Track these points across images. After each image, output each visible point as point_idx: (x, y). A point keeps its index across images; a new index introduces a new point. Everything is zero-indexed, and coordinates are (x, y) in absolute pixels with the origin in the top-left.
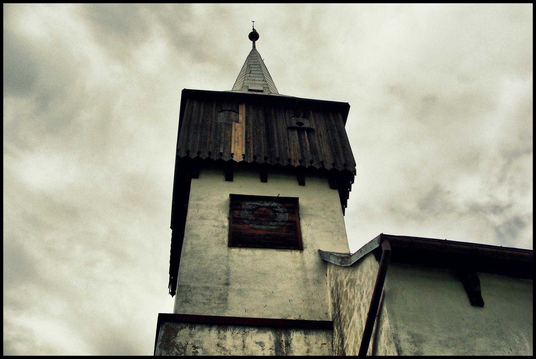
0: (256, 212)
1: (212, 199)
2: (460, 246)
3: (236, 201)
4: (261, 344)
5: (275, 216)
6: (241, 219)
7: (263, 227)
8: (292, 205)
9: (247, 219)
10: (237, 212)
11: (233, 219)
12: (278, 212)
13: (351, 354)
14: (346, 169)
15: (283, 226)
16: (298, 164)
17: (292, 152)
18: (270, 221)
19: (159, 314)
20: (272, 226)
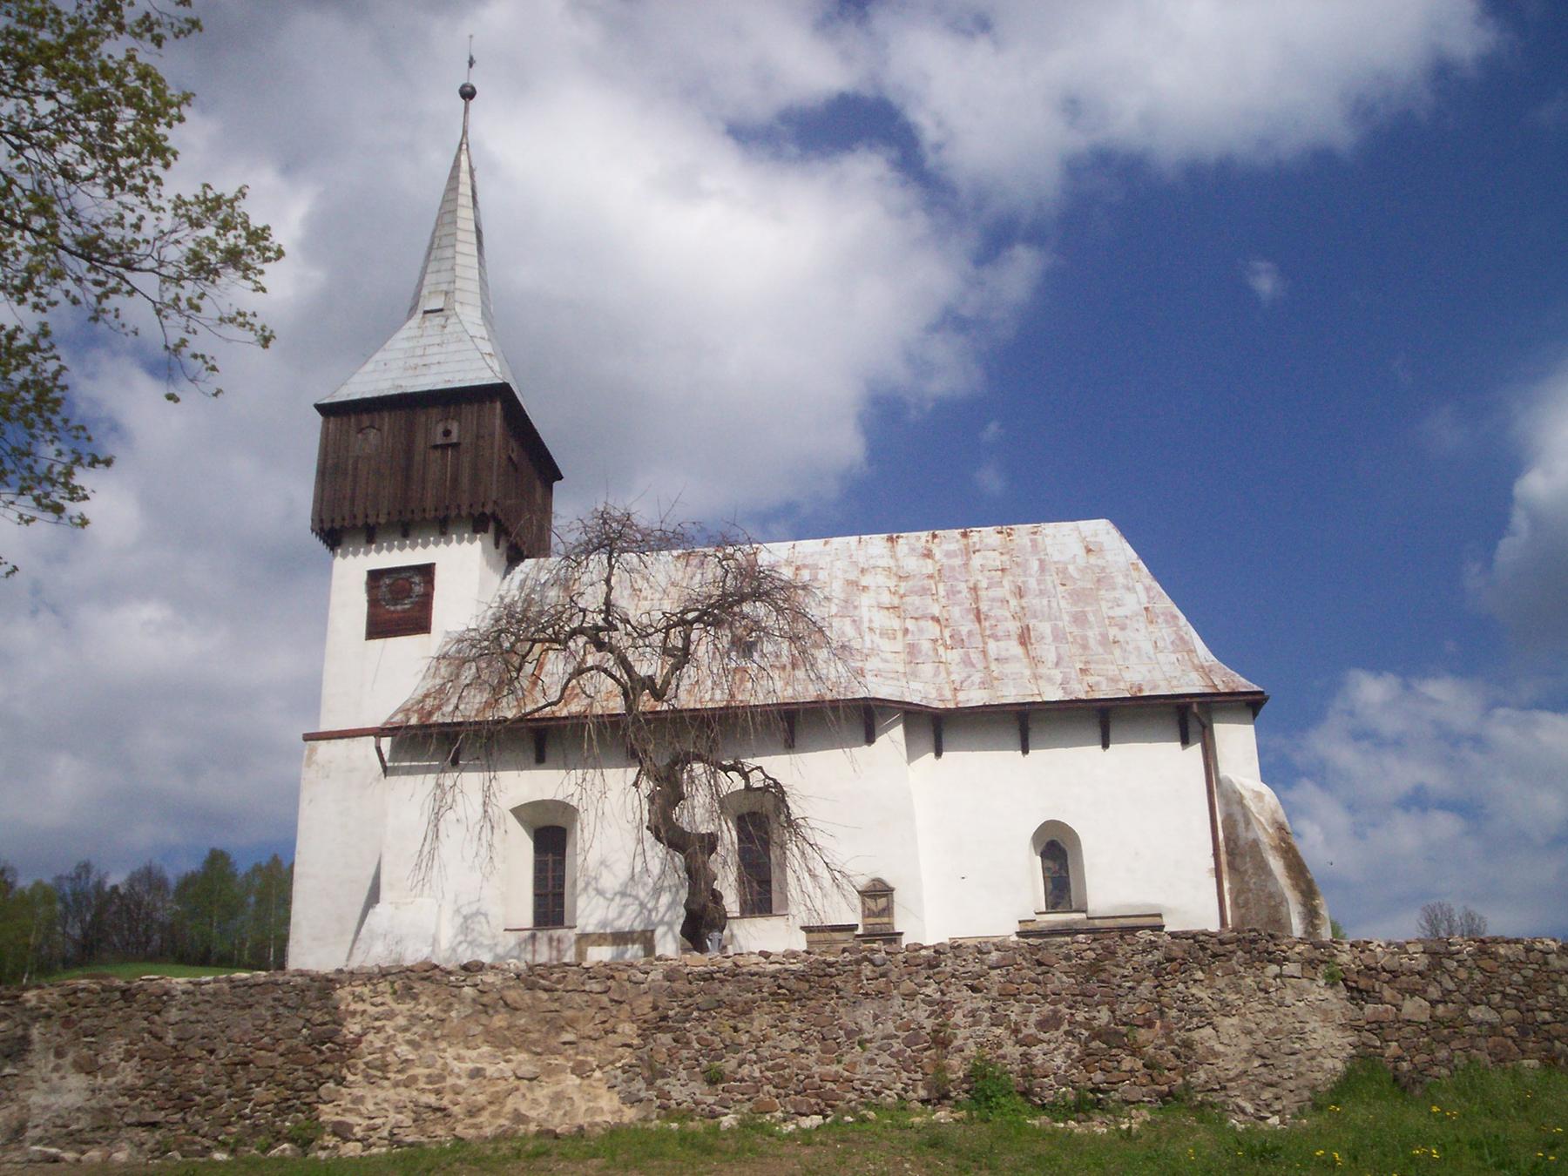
1: (351, 572)
3: (375, 576)
5: (411, 589)
7: (399, 608)
8: (426, 572)
11: (373, 603)
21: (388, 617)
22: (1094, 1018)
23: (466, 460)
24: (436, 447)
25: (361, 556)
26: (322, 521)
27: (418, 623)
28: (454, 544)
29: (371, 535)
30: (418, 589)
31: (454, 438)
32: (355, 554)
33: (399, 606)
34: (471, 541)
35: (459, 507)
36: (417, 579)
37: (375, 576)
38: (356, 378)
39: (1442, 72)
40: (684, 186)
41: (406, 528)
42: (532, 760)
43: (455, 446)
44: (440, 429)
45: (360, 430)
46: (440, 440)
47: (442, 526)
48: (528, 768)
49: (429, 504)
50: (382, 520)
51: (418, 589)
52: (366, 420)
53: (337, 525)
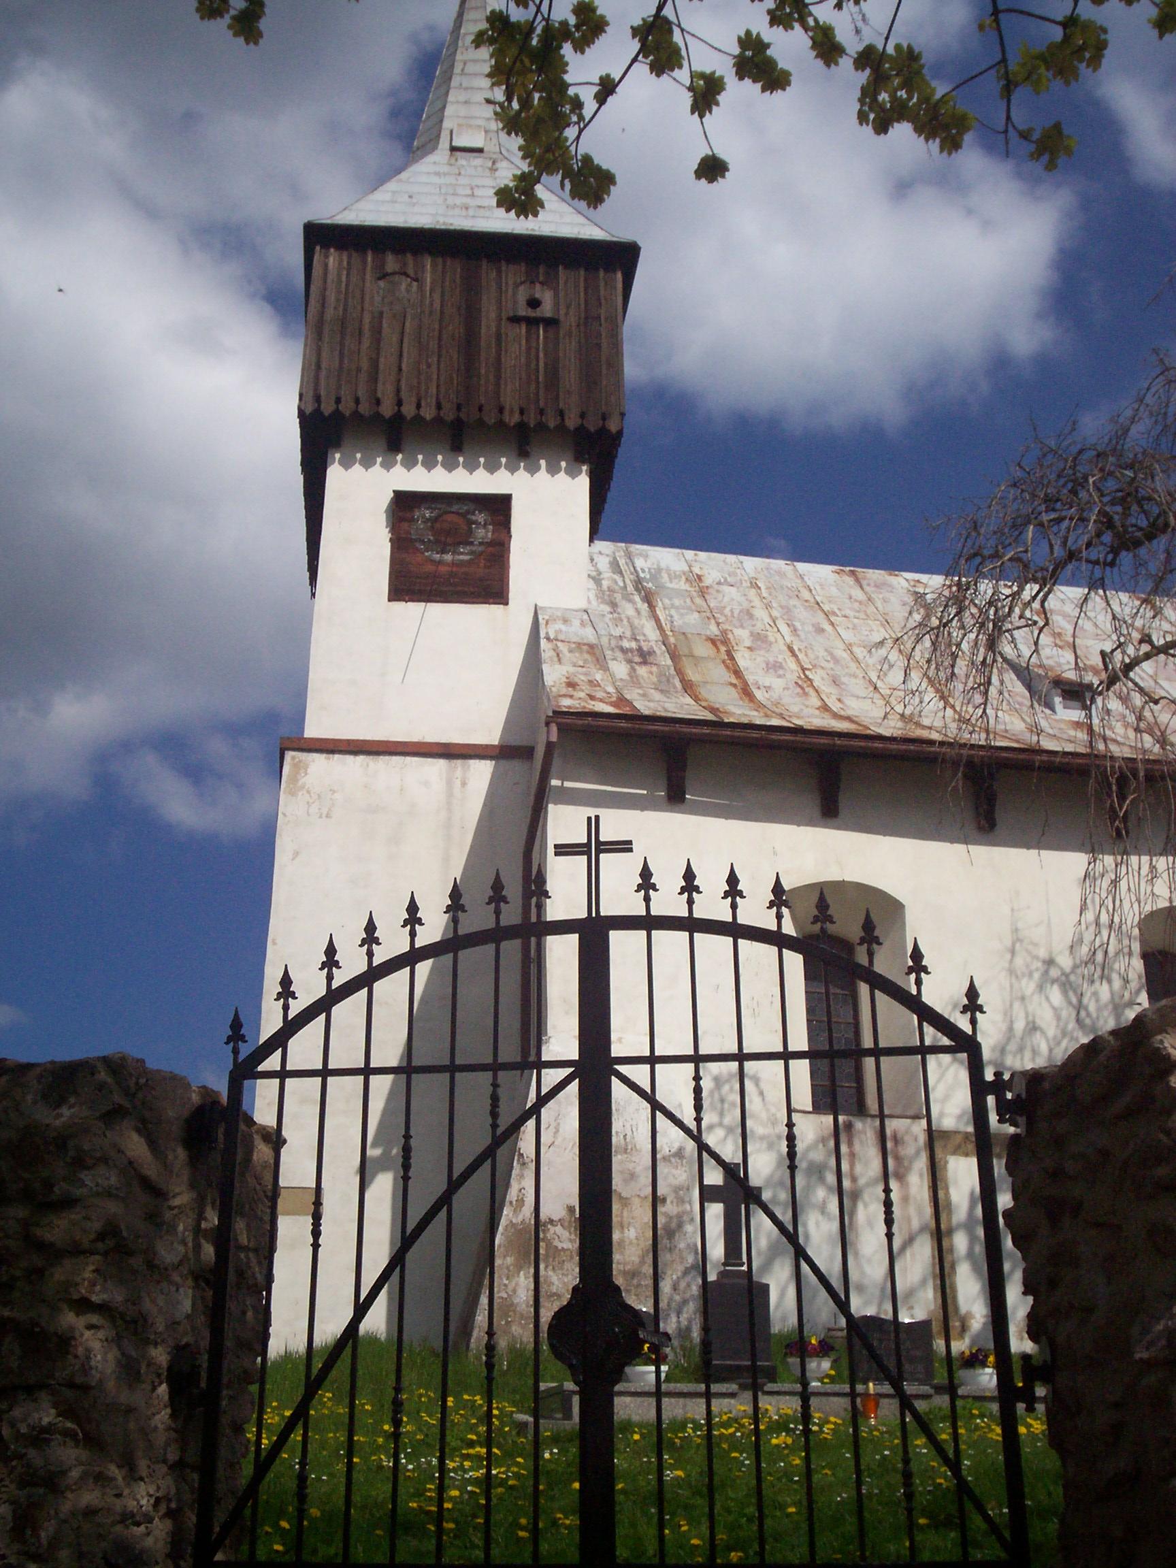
0: (438, 525)
1: (363, 491)
2: (686, 729)
3: (404, 503)
4: (426, 784)
5: (470, 531)
6: (411, 540)
7: (448, 557)
8: (499, 507)
9: (423, 542)
10: (405, 525)
11: (401, 543)
12: (475, 522)
13: (263, 1559)
14: (604, 426)
15: (481, 554)
16: (516, 418)
17: (509, 388)
18: (459, 543)
19: (346, 469)
20: (462, 553)
21: (430, 568)
22: (1030, 1409)
23: (569, 350)
24: (515, 320)
25: (377, 469)
26: (318, 398)
27: (486, 583)
28: (543, 474)
29: (394, 435)
30: (483, 534)
31: (547, 310)
32: (367, 464)
33: (449, 556)
34: (572, 473)
35: (561, 414)
36: (481, 517)
37: (404, 503)
38: (362, 205)
39: (999, 362)
40: (200, 339)
41: (458, 435)
42: (817, 812)
43: (551, 323)
44: (522, 295)
45: (384, 276)
46: (523, 311)
47: (524, 441)
48: (811, 823)
49: (510, 398)
50: (428, 413)
51: (483, 534)
52: (391, 262)
53: (347, 408)
